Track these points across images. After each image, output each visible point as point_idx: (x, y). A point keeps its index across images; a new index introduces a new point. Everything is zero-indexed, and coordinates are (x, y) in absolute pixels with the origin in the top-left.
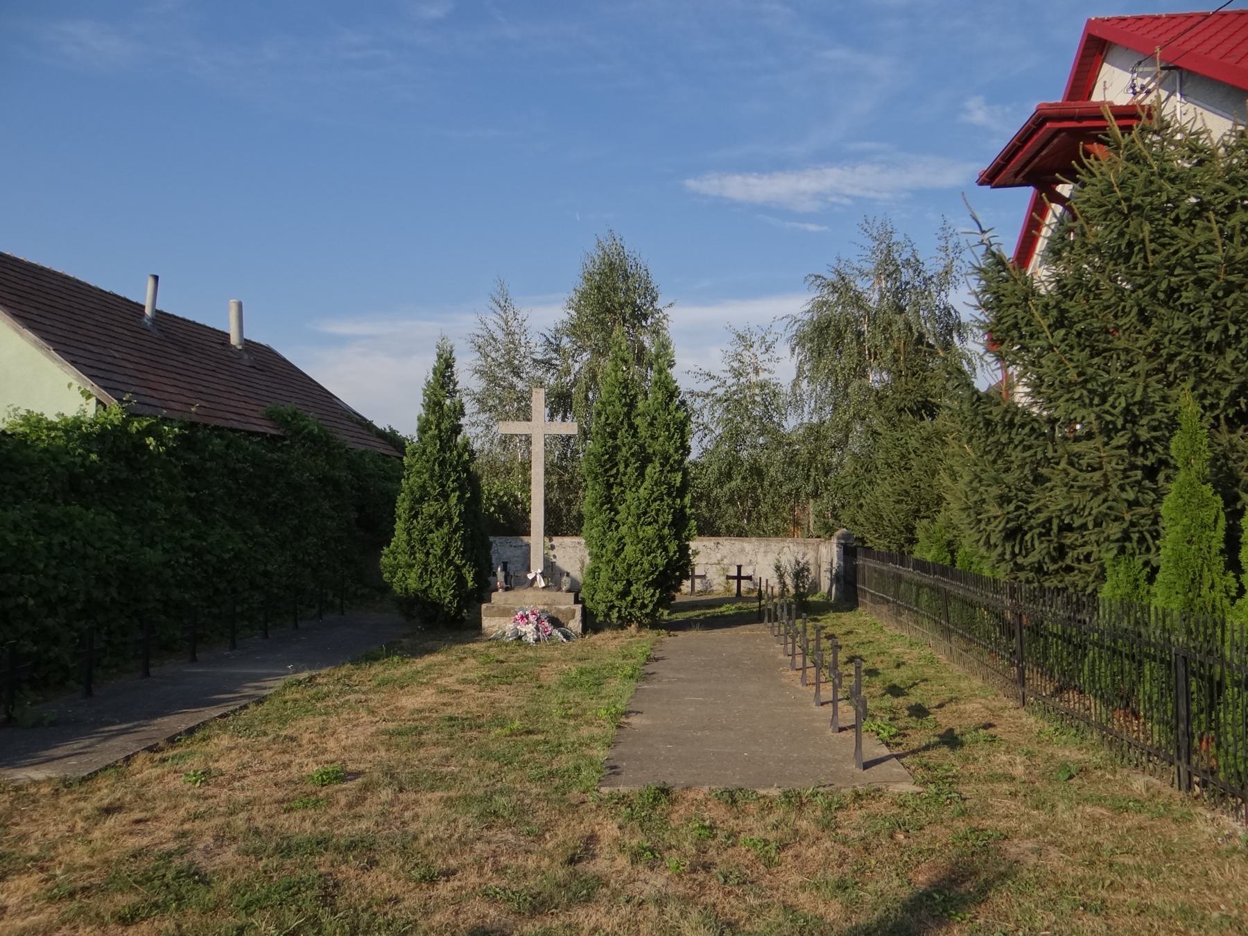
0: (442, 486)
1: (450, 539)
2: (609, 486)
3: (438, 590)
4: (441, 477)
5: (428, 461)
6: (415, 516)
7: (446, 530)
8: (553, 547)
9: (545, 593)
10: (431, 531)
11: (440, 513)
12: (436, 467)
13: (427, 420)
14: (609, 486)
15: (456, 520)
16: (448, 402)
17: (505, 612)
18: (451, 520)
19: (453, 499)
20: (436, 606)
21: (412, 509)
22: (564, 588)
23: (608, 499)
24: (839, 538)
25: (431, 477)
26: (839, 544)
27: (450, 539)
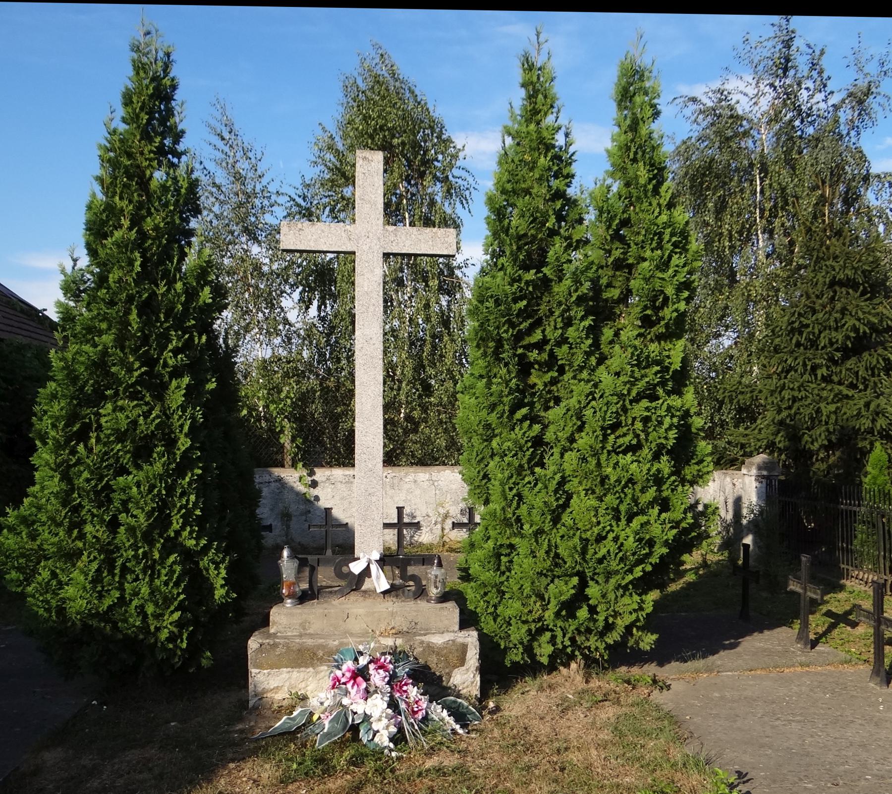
0: (150, 362)
1: (170, 490)
2: (525, 368)
3: (141, 610)
4: (145, 340)
5: (112, 303)
6: (82, 436)
7: (158, 467)
8: (314, 484)
9: (391, 605)
10: (123, 471)
11: (143, 427)
12: (134, 316)
13: (109, 208)
14: (525, 368)
15: (184, 443)
16: (159, 176)
17: (304, 657)
18: (171, 443)
19: (176, 396)
20: (139, 646)
21: (72, 417)
22: (434, 592)
23: (523, 396)
24: (760, 468)
25: (120, 342)
26: (759, 478)
27: (170, 490)
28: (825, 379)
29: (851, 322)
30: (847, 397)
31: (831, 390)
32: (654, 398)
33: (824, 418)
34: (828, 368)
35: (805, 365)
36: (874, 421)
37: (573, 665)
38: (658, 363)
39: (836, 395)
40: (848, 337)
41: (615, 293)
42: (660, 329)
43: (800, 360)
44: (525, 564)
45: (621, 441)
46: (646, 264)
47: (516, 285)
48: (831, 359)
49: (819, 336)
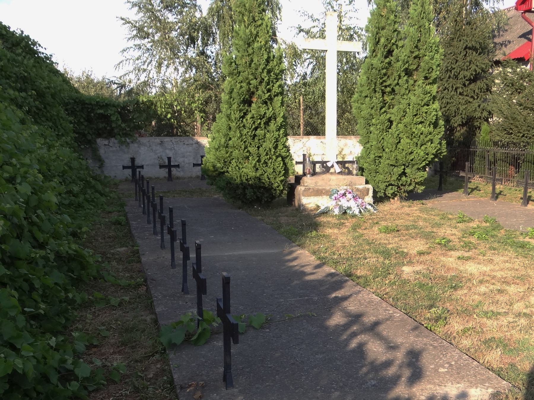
2: (384, 93)
17: (318, 193)
28: (461, 94)
29: (473, 67)
30: (469, 102)
31: (463, 99)
32: (428, 105)
33: (460, 112)
34: (462, 88)
35: (452, 87)
36: (482, 113)
37: (396, 199)
38: (429, 93)
39: (465, 101)
40: (472, 74)
41: (414, 67)
42: (430, 81)
43: (451, 85)
44: (384, 162)
45: (418, 120)
46: (427, 57)
47: (382, 64)
48: (464, 85)
49: (459, 73)
